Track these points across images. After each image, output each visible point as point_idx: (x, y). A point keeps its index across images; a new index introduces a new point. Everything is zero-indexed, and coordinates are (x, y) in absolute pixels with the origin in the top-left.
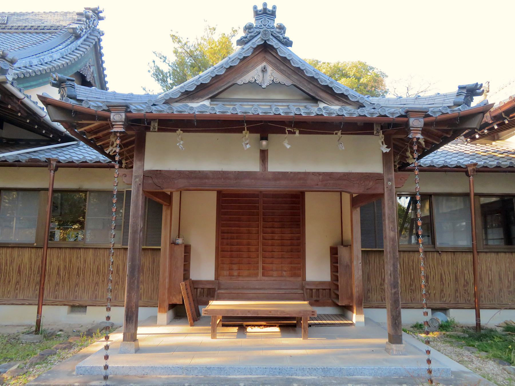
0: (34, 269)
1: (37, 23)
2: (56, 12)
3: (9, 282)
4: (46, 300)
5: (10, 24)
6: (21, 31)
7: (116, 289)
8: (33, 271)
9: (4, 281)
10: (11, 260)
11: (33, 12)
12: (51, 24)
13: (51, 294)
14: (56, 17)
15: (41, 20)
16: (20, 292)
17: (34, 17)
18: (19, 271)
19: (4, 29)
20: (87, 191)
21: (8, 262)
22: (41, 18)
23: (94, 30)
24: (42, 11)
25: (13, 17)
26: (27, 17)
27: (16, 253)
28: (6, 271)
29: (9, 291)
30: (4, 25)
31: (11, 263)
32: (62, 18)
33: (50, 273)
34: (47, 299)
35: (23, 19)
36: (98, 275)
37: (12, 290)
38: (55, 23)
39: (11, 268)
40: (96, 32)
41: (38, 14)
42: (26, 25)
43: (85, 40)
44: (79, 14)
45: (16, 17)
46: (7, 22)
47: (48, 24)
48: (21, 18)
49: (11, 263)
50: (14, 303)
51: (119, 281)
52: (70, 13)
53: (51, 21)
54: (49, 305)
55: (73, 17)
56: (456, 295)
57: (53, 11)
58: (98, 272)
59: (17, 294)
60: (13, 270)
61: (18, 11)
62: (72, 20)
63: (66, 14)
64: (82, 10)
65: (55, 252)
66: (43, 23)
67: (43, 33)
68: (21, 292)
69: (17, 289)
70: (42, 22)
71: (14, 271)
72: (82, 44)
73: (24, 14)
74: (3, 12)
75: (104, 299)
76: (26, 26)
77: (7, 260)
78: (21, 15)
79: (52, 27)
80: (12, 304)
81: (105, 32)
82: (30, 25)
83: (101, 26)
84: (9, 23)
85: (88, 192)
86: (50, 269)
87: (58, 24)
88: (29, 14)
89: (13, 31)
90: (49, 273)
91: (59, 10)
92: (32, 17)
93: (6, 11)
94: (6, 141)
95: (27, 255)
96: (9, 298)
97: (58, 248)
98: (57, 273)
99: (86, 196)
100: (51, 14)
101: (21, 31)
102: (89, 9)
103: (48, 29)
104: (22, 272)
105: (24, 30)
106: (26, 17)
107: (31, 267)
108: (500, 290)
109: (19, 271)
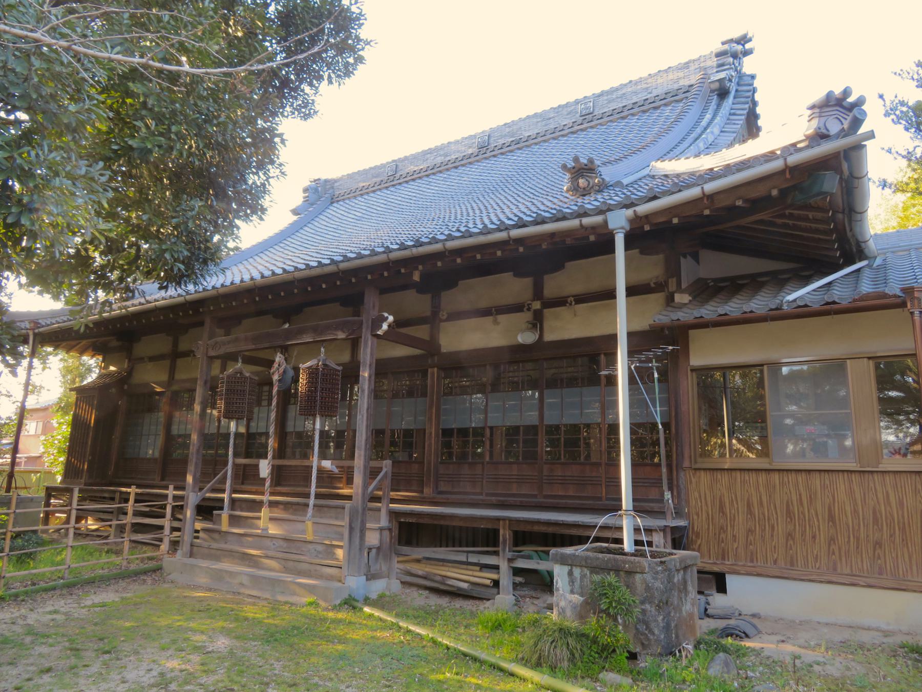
0: (863, 515)
1: (640, 96)
2: (670, 68)
3: (814, 537)
4: (905, 580)
5: (598, 112)
6: (618, 116)
7: (723, 542)
8: (863, 519)
9: (802, 535)
10: (810, 497)
11: (631, 82)
12: (665, 90)
13: (914, 568)
14: (671, 76)
15: (647, 89)
16: (841, 559)
17: (634, 88)
18: (831, 518)
19: (592, 121)
20: (762, 365)
21: (764, 499)
22: (644, 86)
23: (741, 76)
24: (645, 74)
25: (601, 99)
26: (624, 91)
27: (818, 482)
28: (801, 516)
29: (817, 555)
30: (591, 115)
31: (811, 500)
32: (681, 74)
33: (904, 524)
34: (906, 578)
35: (617, 98)
36: (791, 520)
37: (822, 554)
38: (670, 87)
39: (813, 511)
40: (745, 78)
41: (640, 81)
42: (624, 104)
43: (735, 98)
44: (719, 55)
45: (606, 98)
46: (488, 144)
47: (660, 91)
48: (614, 96)
49: (811, 500)
50: (834, 579)
51: (727, 526)
52: (694, 61)
53: (664, 85)
54: (915, 591)
55: (701, 65)
56: (831, 548)
57: (662, 69)
58: (876, 521)
59: (835, 564)
60: (817, 515)
61: (607, 88)
62: (700, 72)
63: (687, 65)
64: (718, 47)
65: (705, 478)
66: (650, 93)
67: (511, 151)
68: (844, 559)
69: (834, 553)
70: (649, 91)
71: (820, 517)
72: (733, 104)
73: (617, 89)
74: (585, 97)
75: (769, 563)
76: (625, 106)
77: (800, 495)
78: (614, 91)
79: (666, 94)
80: (830, 582)
81: (756, 75)
82: (621, 105)
83: (748, 65)
84: (596, 110)
85: (765, 367)
86: (903, 517)
87: (676, 86)
88: (625, 85)
89: (606, 119)
90: (901, 525)
91: (674, 63)
92: (629, 90)
93: (589, 94)
94: (712, 284)
95: (843, 487)
96: (818, 569)
97: (705, 469)
98: (829, 519)
99: (762, 372)
100: (661, 73)
101: (618, 116)
102: (731, 41)
103: (661, 100)
104: (837, 518)
105: (622, 114)
106: (620, 93)
107: (855, 511)
108: (750, 531)
109: (831, 518)
